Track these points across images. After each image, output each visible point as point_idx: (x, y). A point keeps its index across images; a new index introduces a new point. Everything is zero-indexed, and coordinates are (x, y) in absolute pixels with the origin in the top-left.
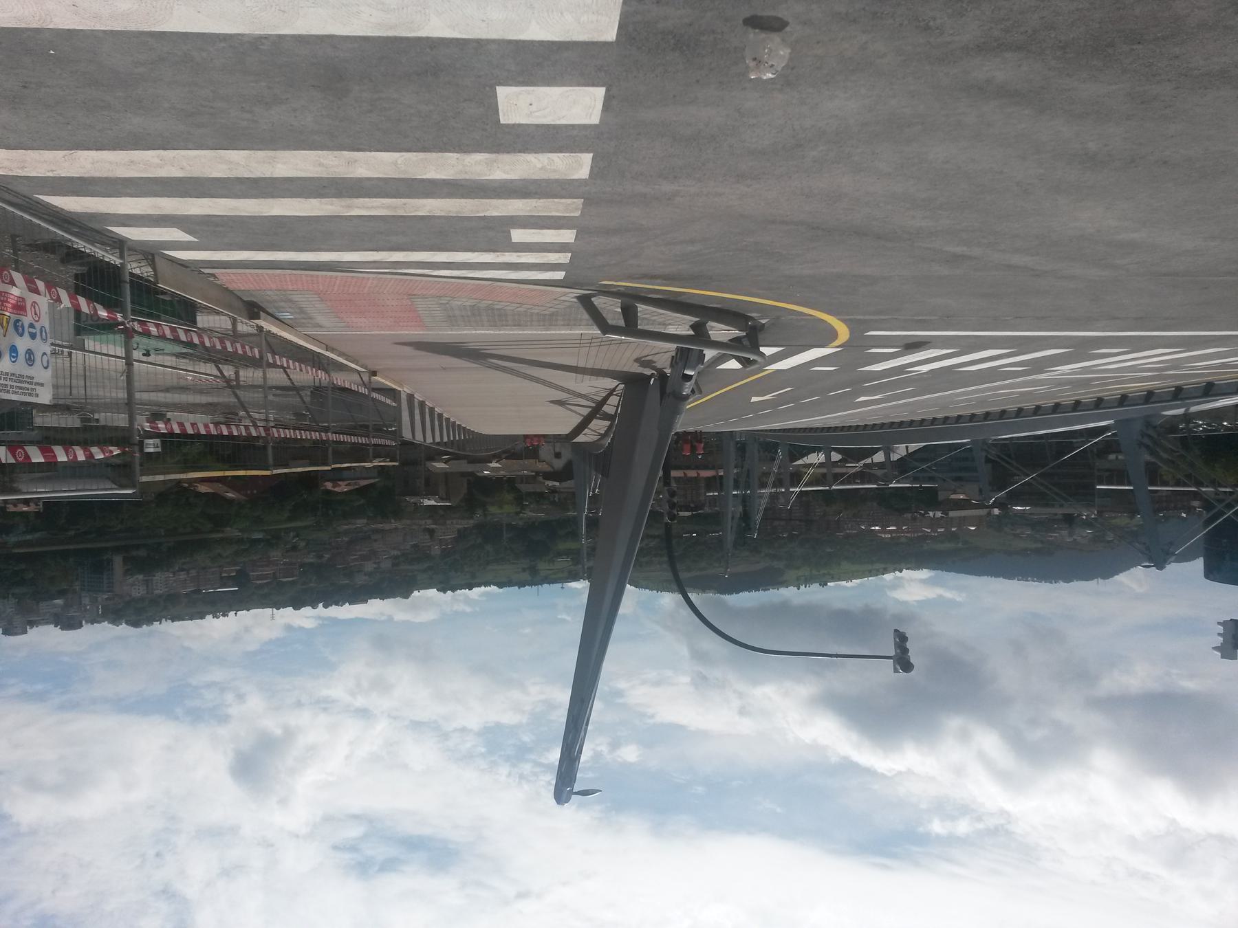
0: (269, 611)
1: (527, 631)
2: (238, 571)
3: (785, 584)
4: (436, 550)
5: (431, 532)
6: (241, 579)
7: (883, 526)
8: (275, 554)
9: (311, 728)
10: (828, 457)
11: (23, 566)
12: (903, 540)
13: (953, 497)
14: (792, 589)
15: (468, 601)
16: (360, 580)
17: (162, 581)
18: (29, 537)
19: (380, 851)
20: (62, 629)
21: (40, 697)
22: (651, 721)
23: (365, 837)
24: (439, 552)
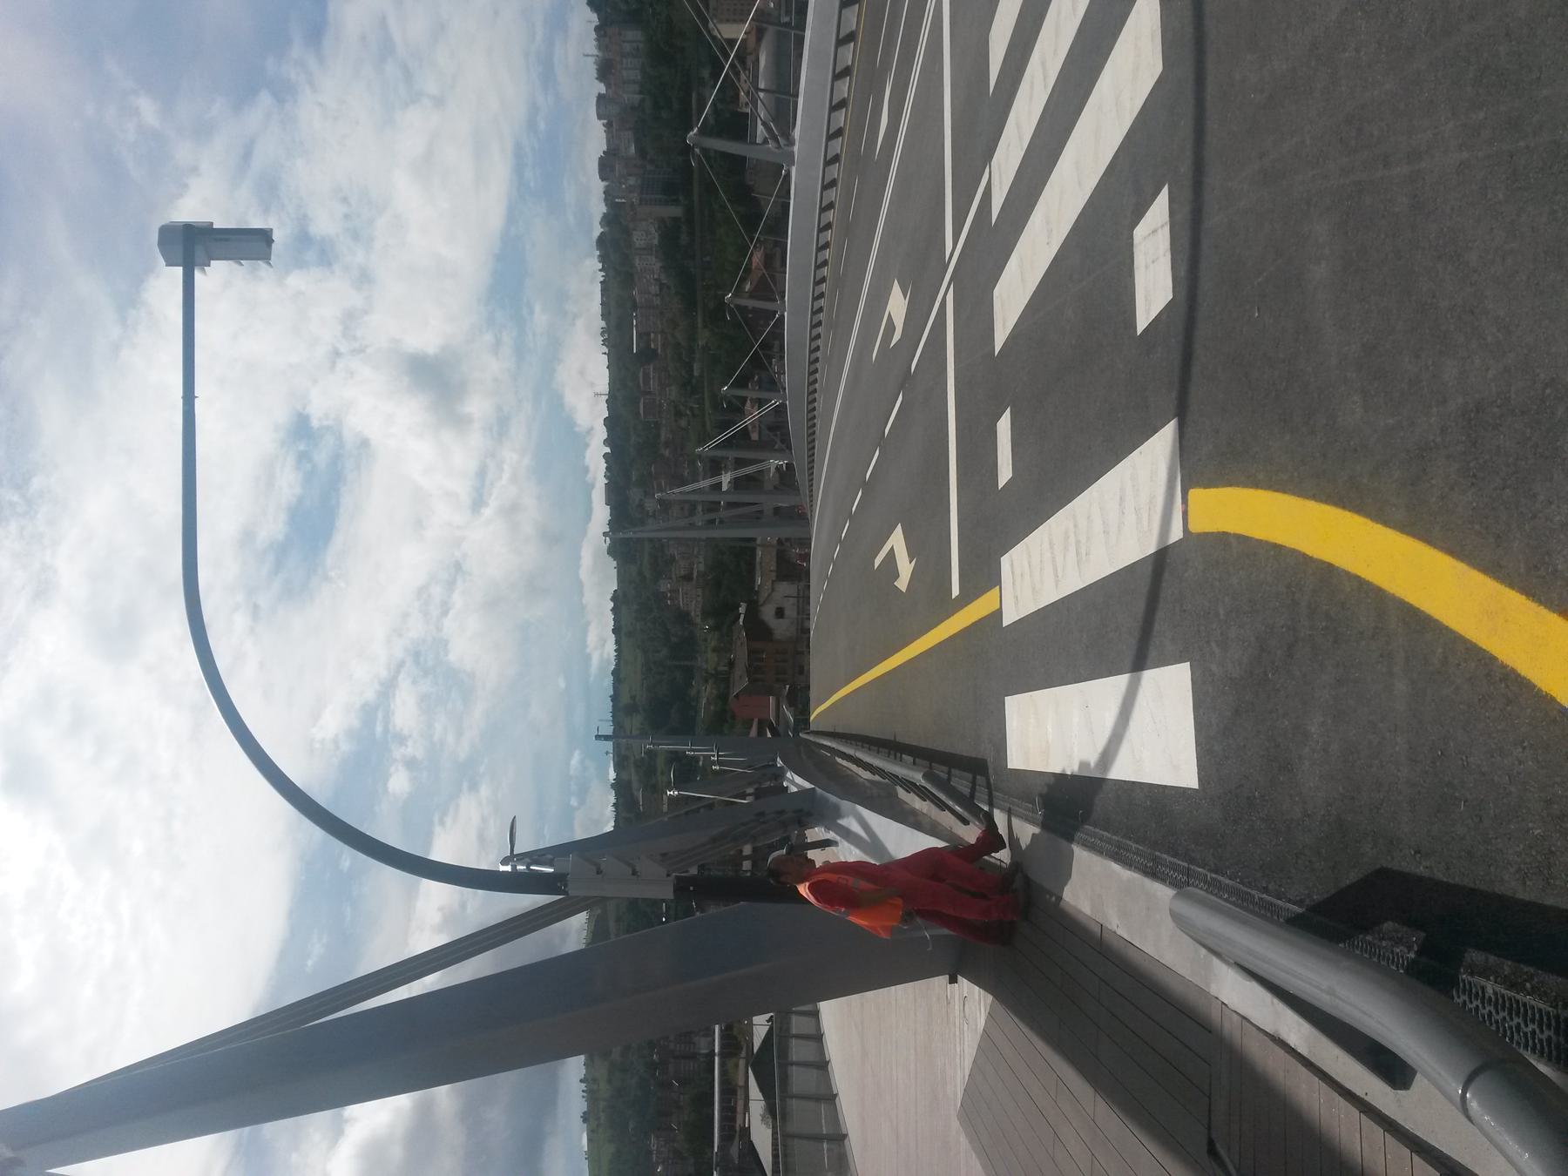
1: (562, 684)
2: (655, 351)
4: (665, 586)
5: (688, 578)
6: (647, 355)
8: (673, 392)
9: (464, 453)
15: (604, 641)
16: (635, 494)
17: (650, 267)
19: (321, 458)
20: (601, 159)
21: (531, 124)
22: (436, 819)
24: (663, 589)
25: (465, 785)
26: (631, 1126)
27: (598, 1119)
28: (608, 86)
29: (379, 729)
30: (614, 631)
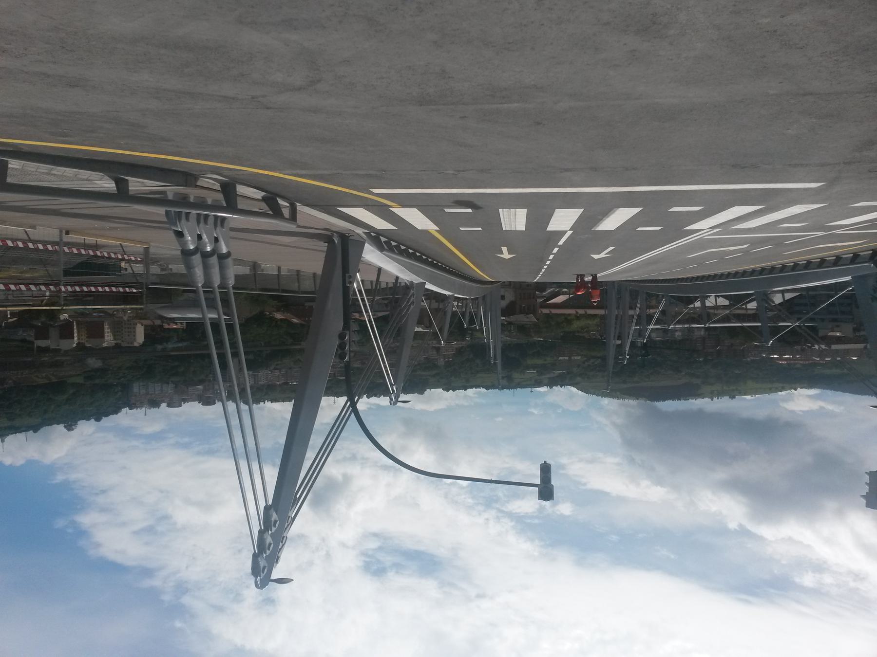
0: (332, 398)
1: (500, 419)
3: (702, 396)
4: (441, 362)
7: (781, 355)
10: (703, 303)
11: (177, 364)
12: (798, 366)
13: (831, 334)
14: (707, 400)
18: (180, 345)
19: (387, 559)
21: (186, 446)
22: (583, 488)
23: (380, 549)
25: (562, 472)
26: (737, 372)
27: (733, 390)
28: (164, 402)
29: (536, 521)
30: (466, 390)
